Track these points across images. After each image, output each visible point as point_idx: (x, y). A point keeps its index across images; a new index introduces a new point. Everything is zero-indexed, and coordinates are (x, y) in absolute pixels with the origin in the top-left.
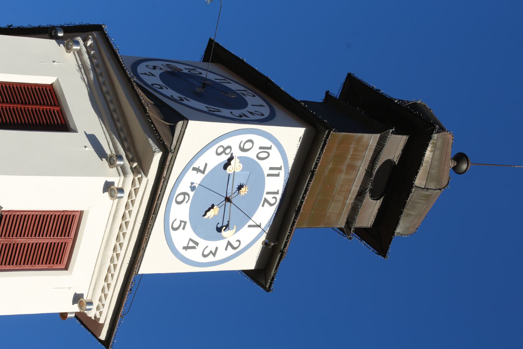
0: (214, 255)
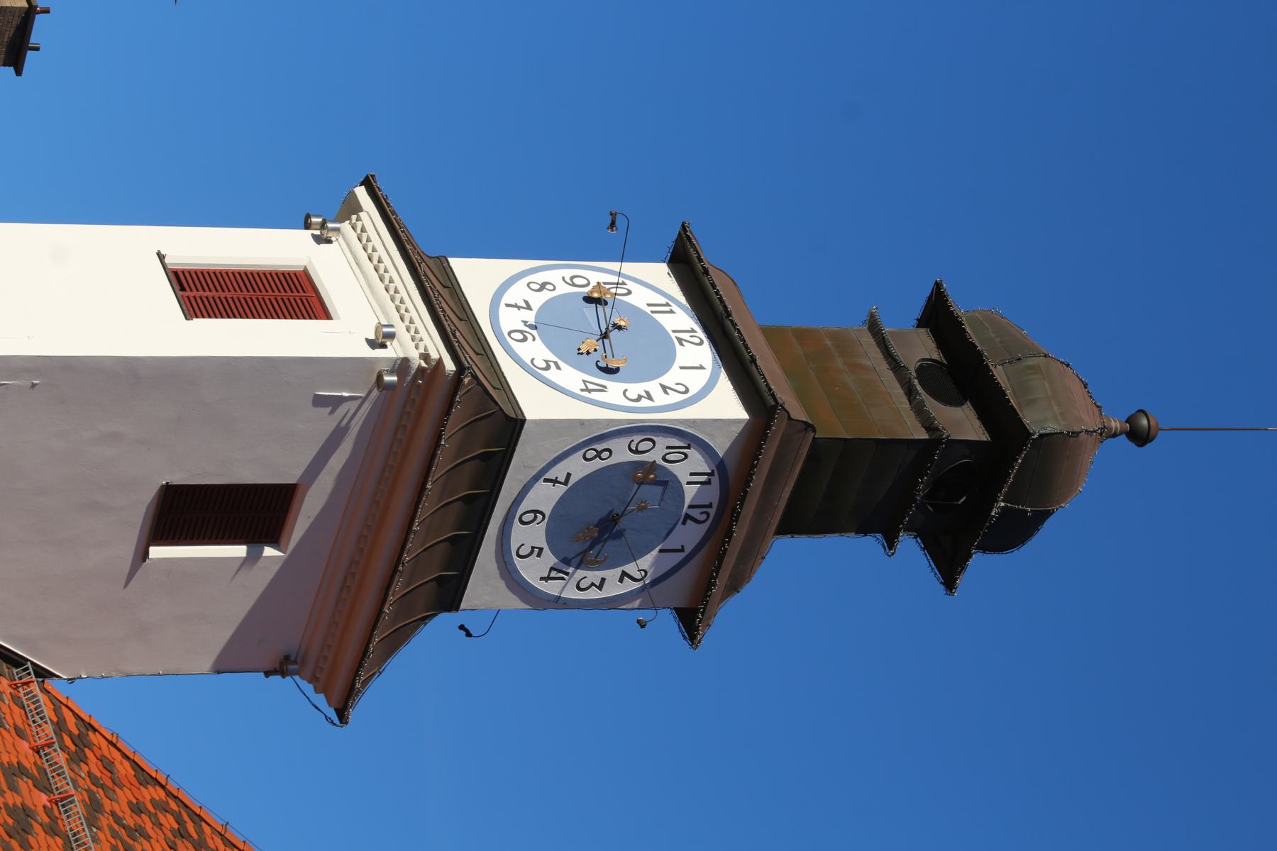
0: (600, 587)
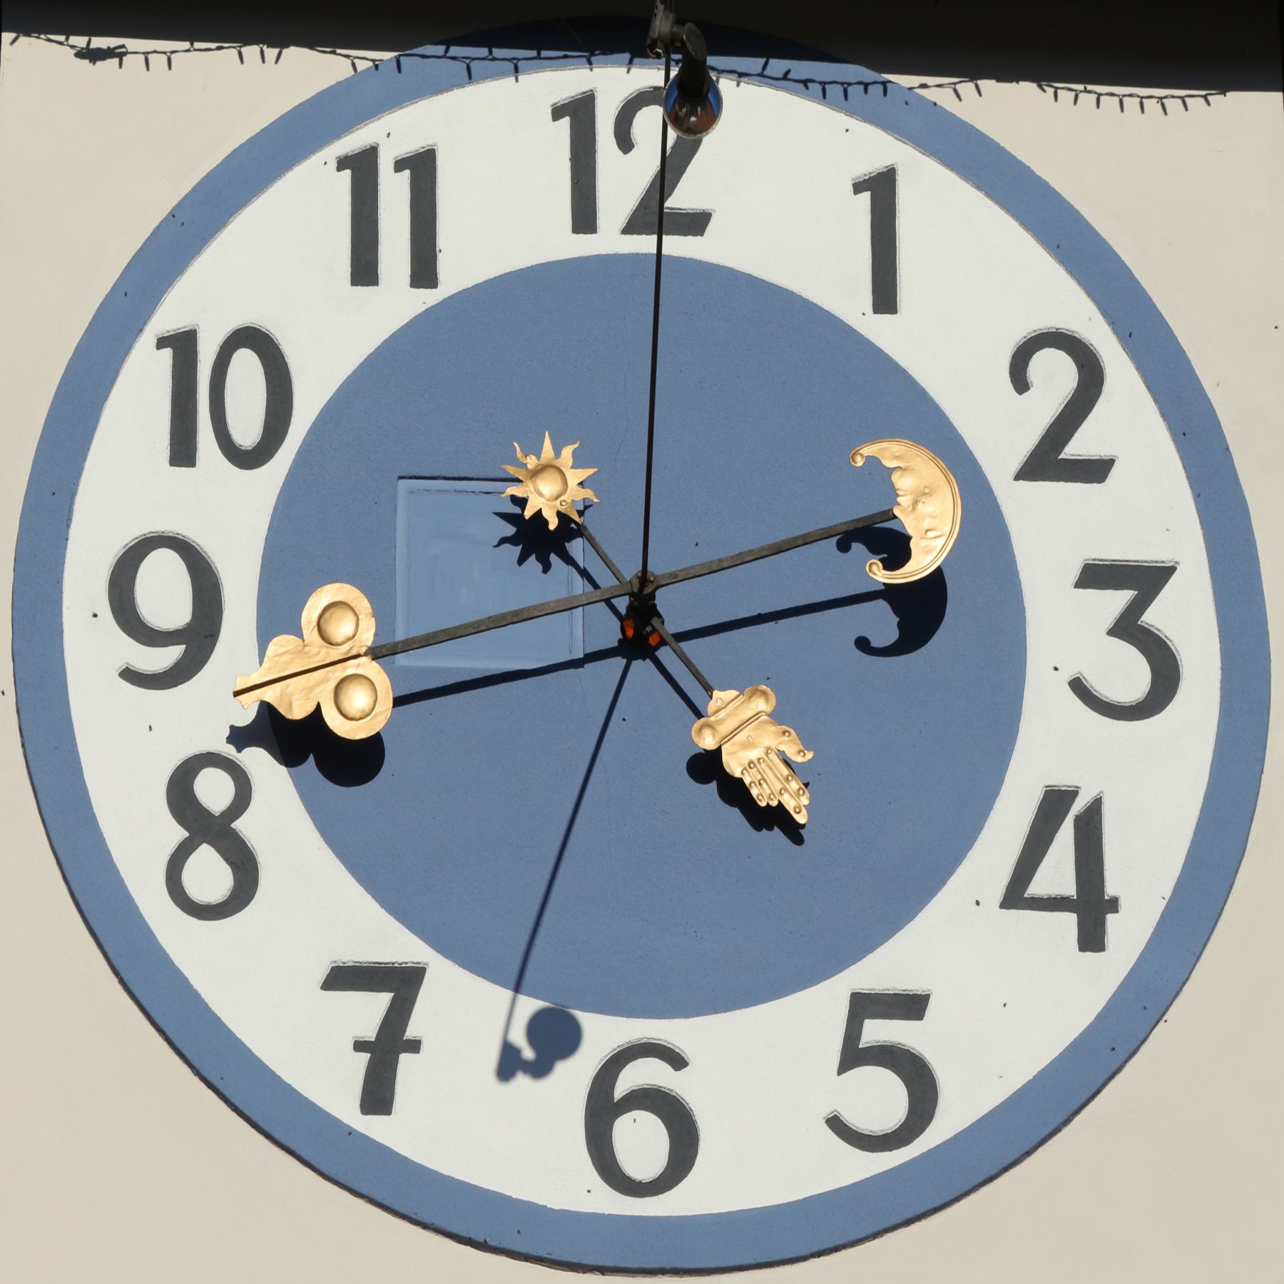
0: (1147, 580)
